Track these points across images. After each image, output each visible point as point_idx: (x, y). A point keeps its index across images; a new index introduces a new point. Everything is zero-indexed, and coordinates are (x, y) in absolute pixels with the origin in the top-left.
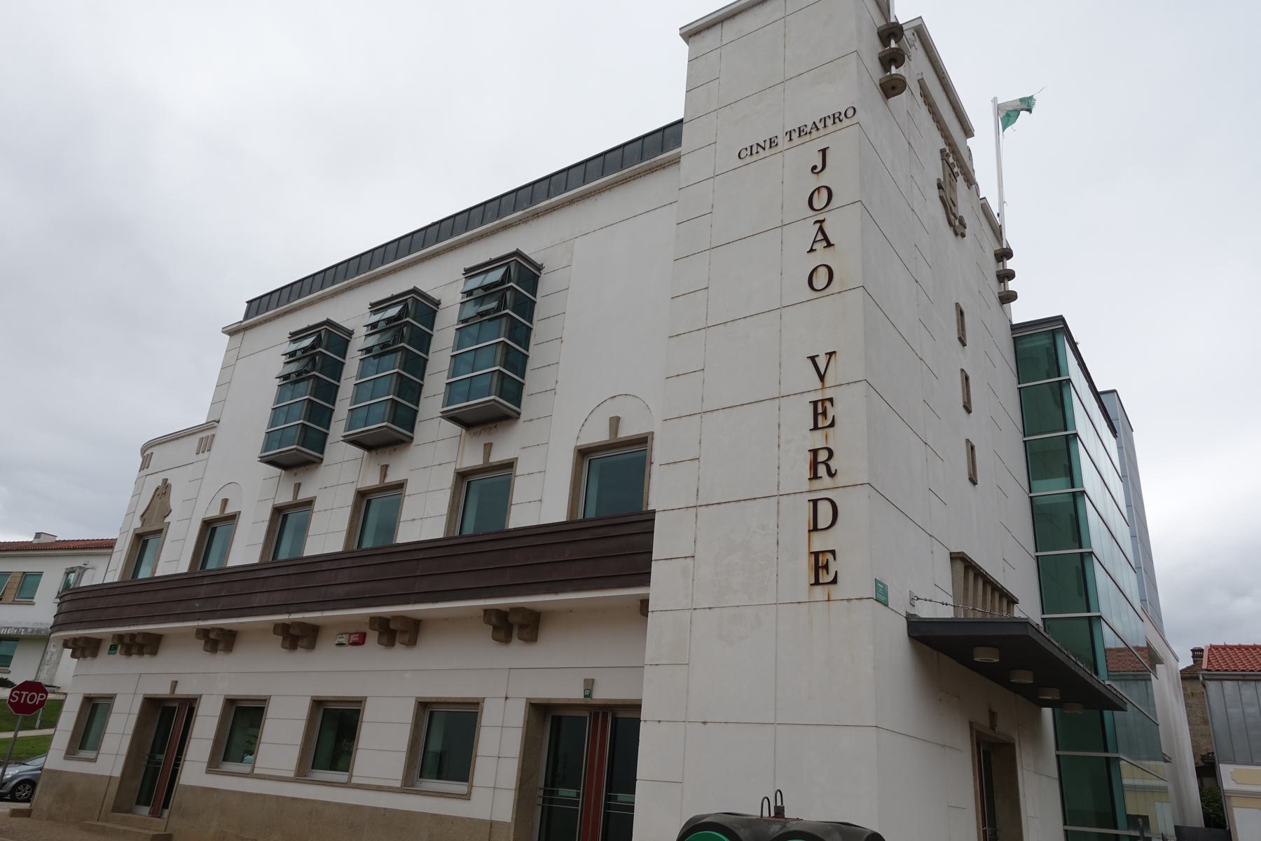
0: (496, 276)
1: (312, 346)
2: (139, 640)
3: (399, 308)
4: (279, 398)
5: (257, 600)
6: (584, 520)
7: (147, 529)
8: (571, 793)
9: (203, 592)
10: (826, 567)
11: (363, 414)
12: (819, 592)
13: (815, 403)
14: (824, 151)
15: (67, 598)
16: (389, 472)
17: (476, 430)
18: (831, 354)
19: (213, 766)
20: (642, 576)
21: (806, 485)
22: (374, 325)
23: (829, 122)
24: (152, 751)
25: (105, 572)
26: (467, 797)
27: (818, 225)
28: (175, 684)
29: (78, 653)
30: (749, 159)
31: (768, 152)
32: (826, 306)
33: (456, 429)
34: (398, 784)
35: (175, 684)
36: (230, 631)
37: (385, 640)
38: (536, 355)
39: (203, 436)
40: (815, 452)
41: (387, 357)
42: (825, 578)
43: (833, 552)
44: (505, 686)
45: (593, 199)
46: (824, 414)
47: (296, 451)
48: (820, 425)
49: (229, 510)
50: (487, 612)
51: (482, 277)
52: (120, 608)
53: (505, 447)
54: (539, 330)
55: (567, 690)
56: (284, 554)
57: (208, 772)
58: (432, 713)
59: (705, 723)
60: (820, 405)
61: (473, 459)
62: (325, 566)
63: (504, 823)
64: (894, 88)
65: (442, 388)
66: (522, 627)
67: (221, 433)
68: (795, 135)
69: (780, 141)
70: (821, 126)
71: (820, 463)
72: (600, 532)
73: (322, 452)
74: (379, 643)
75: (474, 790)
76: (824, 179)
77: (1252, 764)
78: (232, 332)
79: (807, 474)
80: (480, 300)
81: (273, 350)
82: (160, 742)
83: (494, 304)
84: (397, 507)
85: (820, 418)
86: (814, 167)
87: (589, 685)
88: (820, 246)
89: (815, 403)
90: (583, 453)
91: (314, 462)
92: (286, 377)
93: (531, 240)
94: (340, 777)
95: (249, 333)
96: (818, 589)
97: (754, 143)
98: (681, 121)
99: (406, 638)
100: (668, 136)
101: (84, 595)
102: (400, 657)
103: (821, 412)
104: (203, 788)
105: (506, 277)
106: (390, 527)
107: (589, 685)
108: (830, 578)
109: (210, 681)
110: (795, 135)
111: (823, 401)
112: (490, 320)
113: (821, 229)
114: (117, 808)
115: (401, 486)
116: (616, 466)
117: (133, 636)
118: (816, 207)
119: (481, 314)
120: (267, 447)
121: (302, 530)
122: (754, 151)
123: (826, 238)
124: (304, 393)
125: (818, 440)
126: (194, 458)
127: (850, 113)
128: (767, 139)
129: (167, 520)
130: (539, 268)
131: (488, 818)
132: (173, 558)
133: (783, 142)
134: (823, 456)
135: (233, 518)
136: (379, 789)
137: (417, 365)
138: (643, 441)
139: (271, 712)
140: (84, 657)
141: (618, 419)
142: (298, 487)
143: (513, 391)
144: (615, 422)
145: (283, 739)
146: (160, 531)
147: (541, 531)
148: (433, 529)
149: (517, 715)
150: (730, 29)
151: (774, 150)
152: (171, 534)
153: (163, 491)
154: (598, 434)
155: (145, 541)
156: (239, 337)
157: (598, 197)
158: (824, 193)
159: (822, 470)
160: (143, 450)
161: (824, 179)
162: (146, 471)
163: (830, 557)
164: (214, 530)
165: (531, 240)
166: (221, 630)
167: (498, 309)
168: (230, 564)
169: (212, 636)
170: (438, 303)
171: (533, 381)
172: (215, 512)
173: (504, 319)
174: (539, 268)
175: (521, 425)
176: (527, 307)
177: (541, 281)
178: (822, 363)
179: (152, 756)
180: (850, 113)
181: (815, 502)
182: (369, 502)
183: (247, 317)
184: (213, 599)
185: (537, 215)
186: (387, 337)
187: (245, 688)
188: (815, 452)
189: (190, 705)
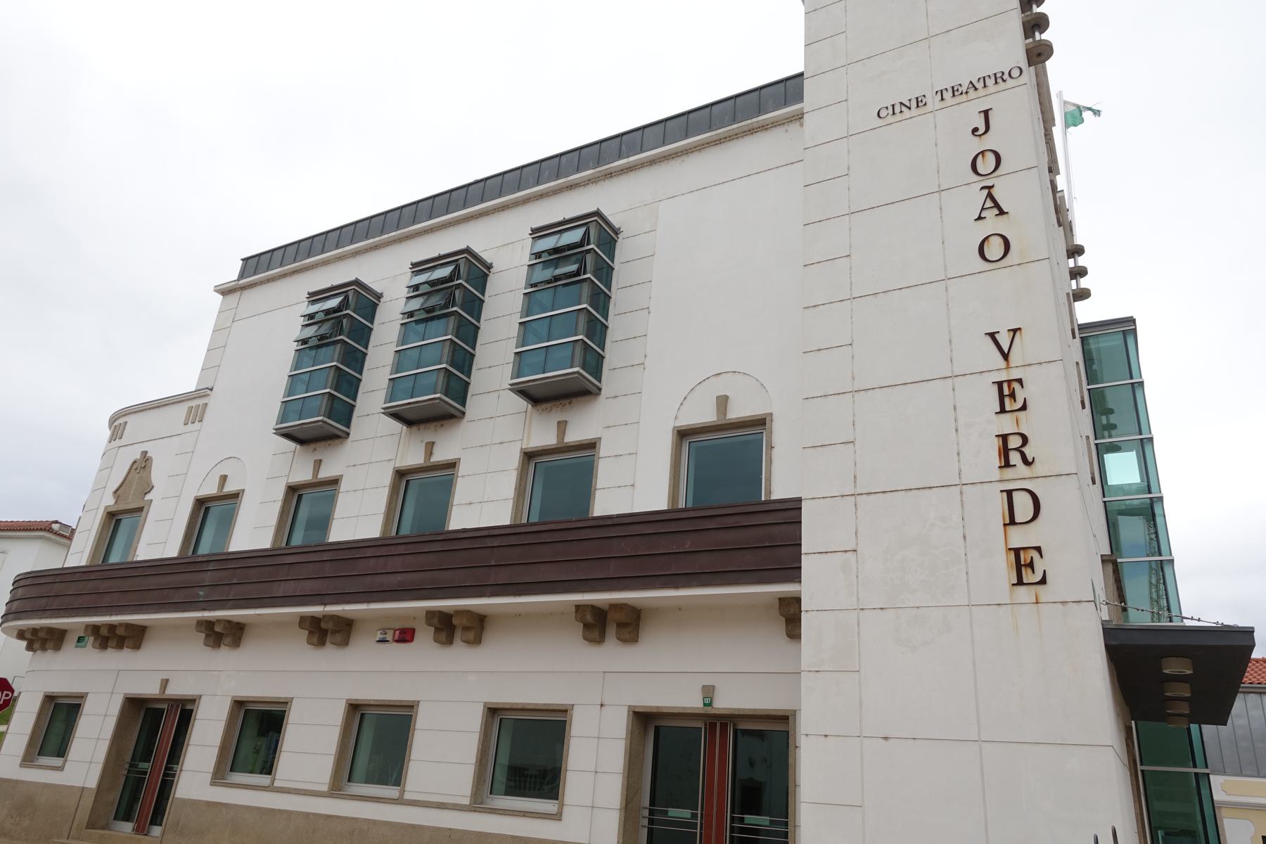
0: (444, 272)
1: (338, 309)
2: (120, 632)
3: (582, 230)
4: (297, 364)
5: (280, 590)
6: (528, 524)
7: (122, 507)
8: (685, 814)
9: (207, 578)
10: (1031, 565)
11: (298, 406)
12: (1023, 593)
13: (1000, 385)
14: (986, 113)
15: (22, 583)
16: (435, 450)
17: (544, 406)
18: (1015, 331)
19: (218, 777)
20: (792, 572)
21: (996, 474)
22: (311, 316)
23: (990, 82)
24: (133, 759)
25: (79, 555)
26: (557, 817)
27: (986, 192)
28: (165, 683)
29: (36, 645)
30: (890, 119)
31: (914, 111)
32: (1002, 279)
33: (521, 403)
34: (466, 801)
35: (165, 683)
36: (238, 624)
37: (315, 640)
38: (617, 325)
39: (194, 405)
40: (1004, 438)
41: (324, 349)
42: (1028, 577)
43: (1038, 549)
44: (601, 696)
45: (680, 160)
46: (1012, 395)
47: (318, 423)
48: (1008, 408)
49: (230, 488)
50: (579, 608)
51: (556, 237)
52: (93, 595)
53: (335, 463)
54: (619, 298)
55: (680, 696)
56: (204, 549)
57: (22, 765)
58: (362, 715)
59: (886, 738)
60: (1005, 386)
61: (414, 458)
62: (369, 553)
64: (1039, 55)
65: (385, 383)
66: (466, 629)
67: (213, 402)
68: (948, 95)
69: (928, 100)
70: (980, 85)
71: (1010, 450)
72: (730, 521)
73: (348, 426)
74: (206, 645)
75: (565, 809)
76: (989, 142)
77: (1241, 775)
78: (226, 291)
79: (996, 461)
80: (555, 263)
81: (285, 313)
82: (145, 750)
83: (574, 267)
84: (331, 501)
85: (1007, 400)
86: (975, 130)
87: (709, 692)
88: (990, 214)
89: (1000, 385)
90: (683, 434)
91: (338, 437)
92: (304, 341)
93: (611, 199)
94: (264, 780)
95: (247, 293)
96: (1022, 590)
97: (897, 102)
98: (801, 74)
99: (338, 638)
100: (787, 90)
101: (325, 557)
102: (459, 657)
103: (1007, 394)
105: (455, 275)
106: (323, 523)
107: (709, 692)
108: (1038, 577)
109: (214, 682)
110: (948, 95)
111: (1009, 382)
112: (564, 285)
113: (990, 196)
114: (91, 825)
115: (335, 482)
116: (724, 452)
117: (112, 627)
118: (980, 171)
119: (556, 279)
120: (283, 417)
121: (228, 522)
122: (897, 109)
123: (997, 205)
124: (330, 360)
125: (1006, 424)
126: (181, 428)
127: (1015, 73)
128: (913, 97)
129: (148, 497)
130: (379, 296)
131: (80, 785)
132: (160, 539)
133: (933, 102)
134: (1014, 442)
135: (236, 496)
137: (356, 359)
138: (761, 423)
139: (422, 721)
140: (44, 649)
141: (726, 398)
142: (318, 464)
143: (595, 364)
144: (723, 402)
145: (309, 749)
146: (140, 509)
147: (492, 532)
148: (370, 528)
149: (618, 726)
151: (921, 110)
152: (153, 514)
153: (143, 464)
154: (705, 414)
155: (119, 521)
156: (234, 298)
157: (685, 158)
158: (991, 158)
159: (1015, 458)
160: (113, 420)
161: (989, 142)
162: (118, 443)
163: (1035, 554)
164: (212, 509)
165: (611, 199)
166: (229, 622)
167: (577, 273)
168: (232, 548)
169: (218, 629)
170: (489, 267)
171: (613, 355)
172: (211, 489)
173: (452, 319)
174: (379, 296)
175: (349, 445)
176: (605, 272)
177: (618, 245)
178: (1004, 341)
180: (1015, 73)
181: (1009, 493)
182: (300, 497)
183: (242, 275)
184: (212, 585)
185: (609, 175)
186: (325, 329)
187: (260, 688)
188: (1004, 438)
189: (184, 712)
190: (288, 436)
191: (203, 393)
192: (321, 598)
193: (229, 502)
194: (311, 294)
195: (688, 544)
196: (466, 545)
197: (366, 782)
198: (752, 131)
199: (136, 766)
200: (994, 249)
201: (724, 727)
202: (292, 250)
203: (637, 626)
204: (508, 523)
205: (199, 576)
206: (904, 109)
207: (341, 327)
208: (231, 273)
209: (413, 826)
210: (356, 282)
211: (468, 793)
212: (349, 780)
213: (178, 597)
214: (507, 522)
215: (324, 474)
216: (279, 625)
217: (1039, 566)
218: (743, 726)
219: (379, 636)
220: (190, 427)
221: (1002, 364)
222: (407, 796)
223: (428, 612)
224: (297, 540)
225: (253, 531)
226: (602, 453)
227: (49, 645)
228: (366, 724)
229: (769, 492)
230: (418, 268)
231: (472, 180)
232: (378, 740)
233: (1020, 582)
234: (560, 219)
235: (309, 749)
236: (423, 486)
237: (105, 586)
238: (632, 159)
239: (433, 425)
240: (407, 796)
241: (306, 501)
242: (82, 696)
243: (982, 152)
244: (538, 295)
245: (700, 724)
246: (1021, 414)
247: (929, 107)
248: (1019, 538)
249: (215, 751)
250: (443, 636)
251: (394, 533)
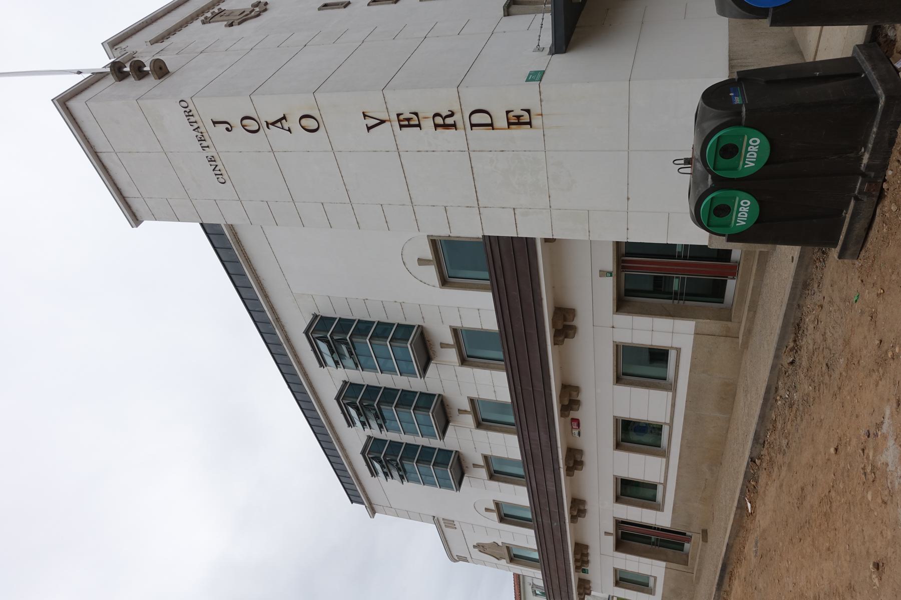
4: (418, 482)
5: (551, 488)
6: (490, 279)
9: (546, 521)
10: (518, 117)
11: (424, 428)
13: (401, 126)
14: (215, 123)
16: (463, 408)
18: (365, 116)
19: (659, 508)
20: (529, 243)
21: (461, 132)
23: (192, 119)
25: (535, 576)
31: (218, 163)
32: (329, 119)
35: (607, 533)
38: (377, 316)
39: (443, 525)
40: (437, 126)
42: (526, 118)
43: (508, 112)
44: (605, 328)
46: (409, 120)
47: (452, 468)
48: (417, 123)
49: (493, 507)
50: (556, 343)
52: (559, 565)
54: (359, 314)
60: (402, 123)
61: (452, 355)
62: (528, 448)
64: (161, 68)
67: (441, 515)
68: (205, 144)
69: (210, 155)
70: (196, 125)
71: (444, 122)
73: (435, 395)
76: (236, 122)
79: (452, 131)
82: (645, 540)
83: (344, 347)
85: (412, 123)
86: (227, 129)
87: (603, 273)
89: (401, 126)
90: (445, 282)
93: (296, 324)
94: (666, 430)
97: (213, 173)
98: (202, 225)
100: (213, 233)
102: (587, 397)
103: (407, 122)
105: (324, 339)
106: (499, 406)
107: (603, 273)
109: (604, 512)
111: (399, 121)
113: (273, 124)
114: (686, 563)
116: (452, 260)
118: (257, 128)
120: (449, 487)
122: (219, 172)
123: (280, 120)
125: (428, 124)
130: (315, 316)
132: (525, 539)
133: (210, 152)
134: (439, 120)
135: (497, 504)
136: (673, 405)
137: (389, 394)
138: (434, 243)
139: (625, 414)
140: (587, 555)
142: (443, 345)
143: (404, 331)
144: (422, 262)
145: (645, 404)
146: (508, 548)
149: (625, 320)
151: (217, 159)
152: (510, 541)
154: (431, 273)
157: (261, 279)
158: (246, 122)
159: (449, 121)
161: (236, 122)
163: (511, 114)
164: (506, 516)
165: (296, 324)
167: (347, 344)
171: (396, 318)
172: (494, 516)
173: (354, 340)
174: (315, 316)
178: (372, 122)
181: (472, 125)
183: (362, 503)
184: (551, 514)
185: (278, 319)
186: (371, 416)
187: (609, 490)
190: (460, 484)
191: (436, 521)
192: (556, 471)
193: (439, 246)
194: (372, 475)
196: (521, 402)
197: (667, 367)
198: (238, 242)
199: (676, 293)
200: (310, 123)
201: (624, 261)
202: (332, 459)
203: (570, 386)
204: (491, 294)
206: (217, 168)
207: (388, 458)
208: (360, 509)
209: (685, 419)
210: (306, 333)
211: (665, 393)
212: (665, 379)
213: (558, 534)
214: (505, 374)
215: (450, 340)
216: (564, 365)
217: (518, 112)
220: (457, 525)
221: (387, 124)
222: (668, 421)
223: (555, 344)
224: (511, 419)
225: (518, 496)
226: (460, 325)
227: (587, 586)
228: (631, 371)
230: (322, 363)
232: (634, 434)
233: (530, 123)
235: (645, 404)
236: (470, 348)
237: (553, 566)
238: (266, 309)
239: (448, 411)
240: (668, 421)
241: (496, 472)
242: (616, 478)
243: (243, 126)
244: (362, 362)
245: (623, 274)
246: (420, 115)
247: (215, 154)
248: (501, 121)
249: (644, 510)
251: (488, 282)
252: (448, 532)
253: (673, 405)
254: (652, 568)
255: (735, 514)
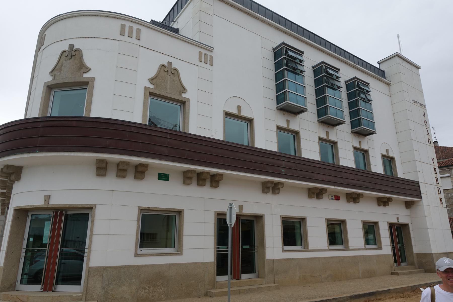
5: (378, 187)
19: (380, 247)
29: (214, 185)
44: (385, 217)
63: (211, 263)
87: (48, 198)
104: (285, 259)
109: (273, 210)
136: (359, 250)
150: (408, 66)
179: (403, 245)
187: (294, 212)
195: (407, 187)
201: (61, 213)
205: (280, 162)
209: (354, 256)
216: (370, 198)
218: (69, 212)
219: (331, 198)
229: (89, 111)
231: (311, 31)
234: (331, 64)
238: (246, 8)
239: (289, 114)
250: (277, 191)
252: (289, 77)
253: (359, 250)
254: (386, 248)
255: (408, 287)
